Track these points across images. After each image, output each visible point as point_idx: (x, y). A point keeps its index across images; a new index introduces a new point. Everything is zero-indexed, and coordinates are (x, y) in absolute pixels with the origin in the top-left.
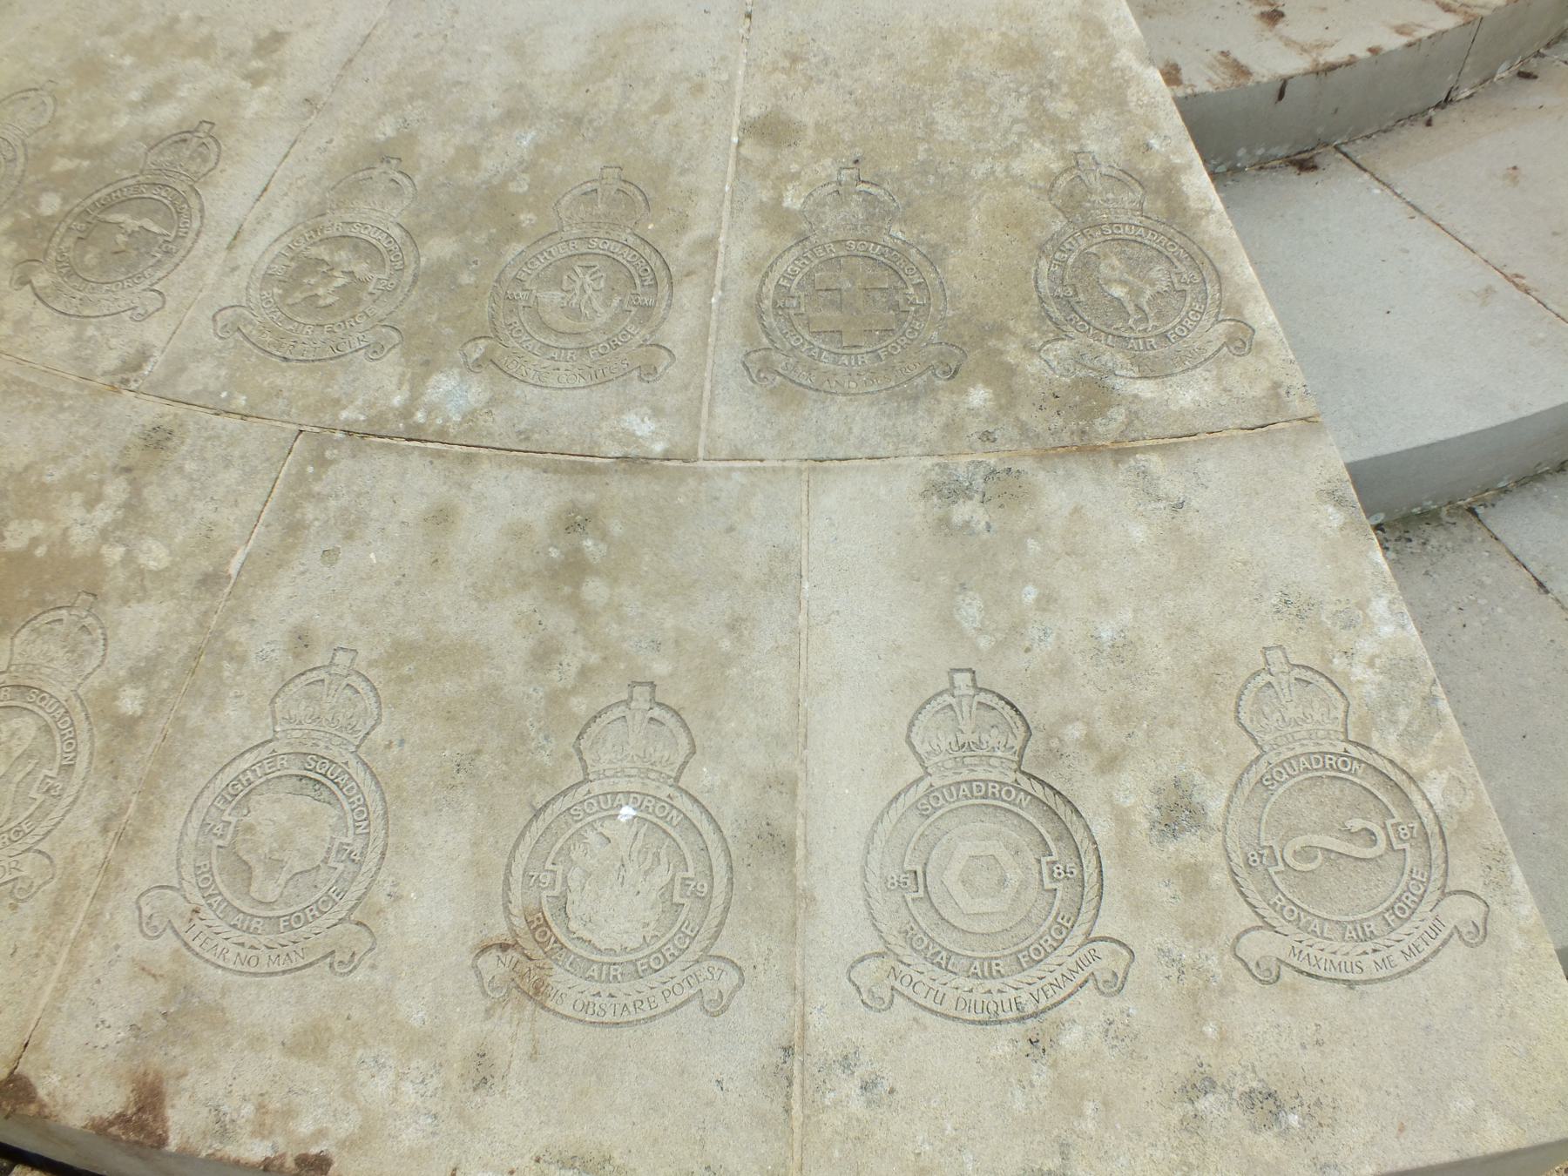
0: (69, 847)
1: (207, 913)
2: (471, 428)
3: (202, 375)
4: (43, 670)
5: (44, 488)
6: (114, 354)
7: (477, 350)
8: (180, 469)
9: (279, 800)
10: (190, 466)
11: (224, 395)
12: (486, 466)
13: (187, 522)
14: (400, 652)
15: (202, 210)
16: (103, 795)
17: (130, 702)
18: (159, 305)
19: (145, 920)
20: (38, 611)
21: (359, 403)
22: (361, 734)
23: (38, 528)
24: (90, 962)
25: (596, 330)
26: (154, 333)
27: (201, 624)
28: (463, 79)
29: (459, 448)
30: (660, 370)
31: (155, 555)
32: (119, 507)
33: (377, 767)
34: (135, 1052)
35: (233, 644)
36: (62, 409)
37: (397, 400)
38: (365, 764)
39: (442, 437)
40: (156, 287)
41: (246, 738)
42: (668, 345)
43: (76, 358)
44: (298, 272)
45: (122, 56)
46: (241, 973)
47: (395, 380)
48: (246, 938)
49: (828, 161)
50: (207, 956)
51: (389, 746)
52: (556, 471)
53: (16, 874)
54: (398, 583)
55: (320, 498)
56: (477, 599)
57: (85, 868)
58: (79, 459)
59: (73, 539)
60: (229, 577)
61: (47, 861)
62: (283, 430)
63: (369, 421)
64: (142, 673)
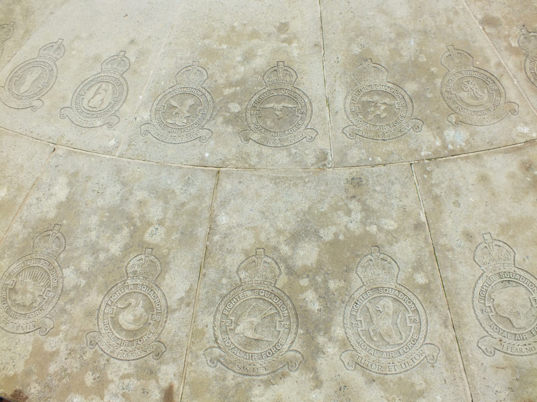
0: (437, 338)
1: (504, 340)
2: (471, 146)
3: (355, 154)
4: (378, 280)
5: (323, 214)
6: (311, 157)
7: (453, 118)
8: (374, 191)
9: (501, 292)
10: (378, 188)
11: (370, 159)
12: (485, 157)
13: (393, 209)
14: (504, 228)
15: (305, 94)
16: (436, 315)
17: (421, 279)
18: (316, 133)
19: (485, 351)
20: (359, 259)
21: (424, 148)
22: (512, 259)
23: (334, 229)
24: (476, 373)
25: (486, 102)
26: (322, 143)
27: (426, 242)
28: (371, 26)
29: (469, 153)
30: (516, 109)
31: (390, 224)
32: (361, 211)
33: (525, 268)
34: (516, 397)
35: (445, 245)
36: (306, 183)
37: (438, 143)
38: (520, 269)
39: (463, 152)
40: (309, 127)
41: (474, 276)
42: (513, 101)
43: (296, 162)
44: (364, 109)
45: (220, 45)
46: (531, 355)
47: (432, 136)
48: (524, 342)
49: (515, 28)
50: (516, 354)
51: (524, 260)
52: (509, 152)
53: (424, 355)
54: (487, 205)
55: (437, 185)
56: (516, 202)
57: (449, 342)
58: (329, 199)
59: (352, 229)
60: (424, 223)
61: (432, 346)
62: (404, 165)
63: (433, 153)
64: (418, 267)
